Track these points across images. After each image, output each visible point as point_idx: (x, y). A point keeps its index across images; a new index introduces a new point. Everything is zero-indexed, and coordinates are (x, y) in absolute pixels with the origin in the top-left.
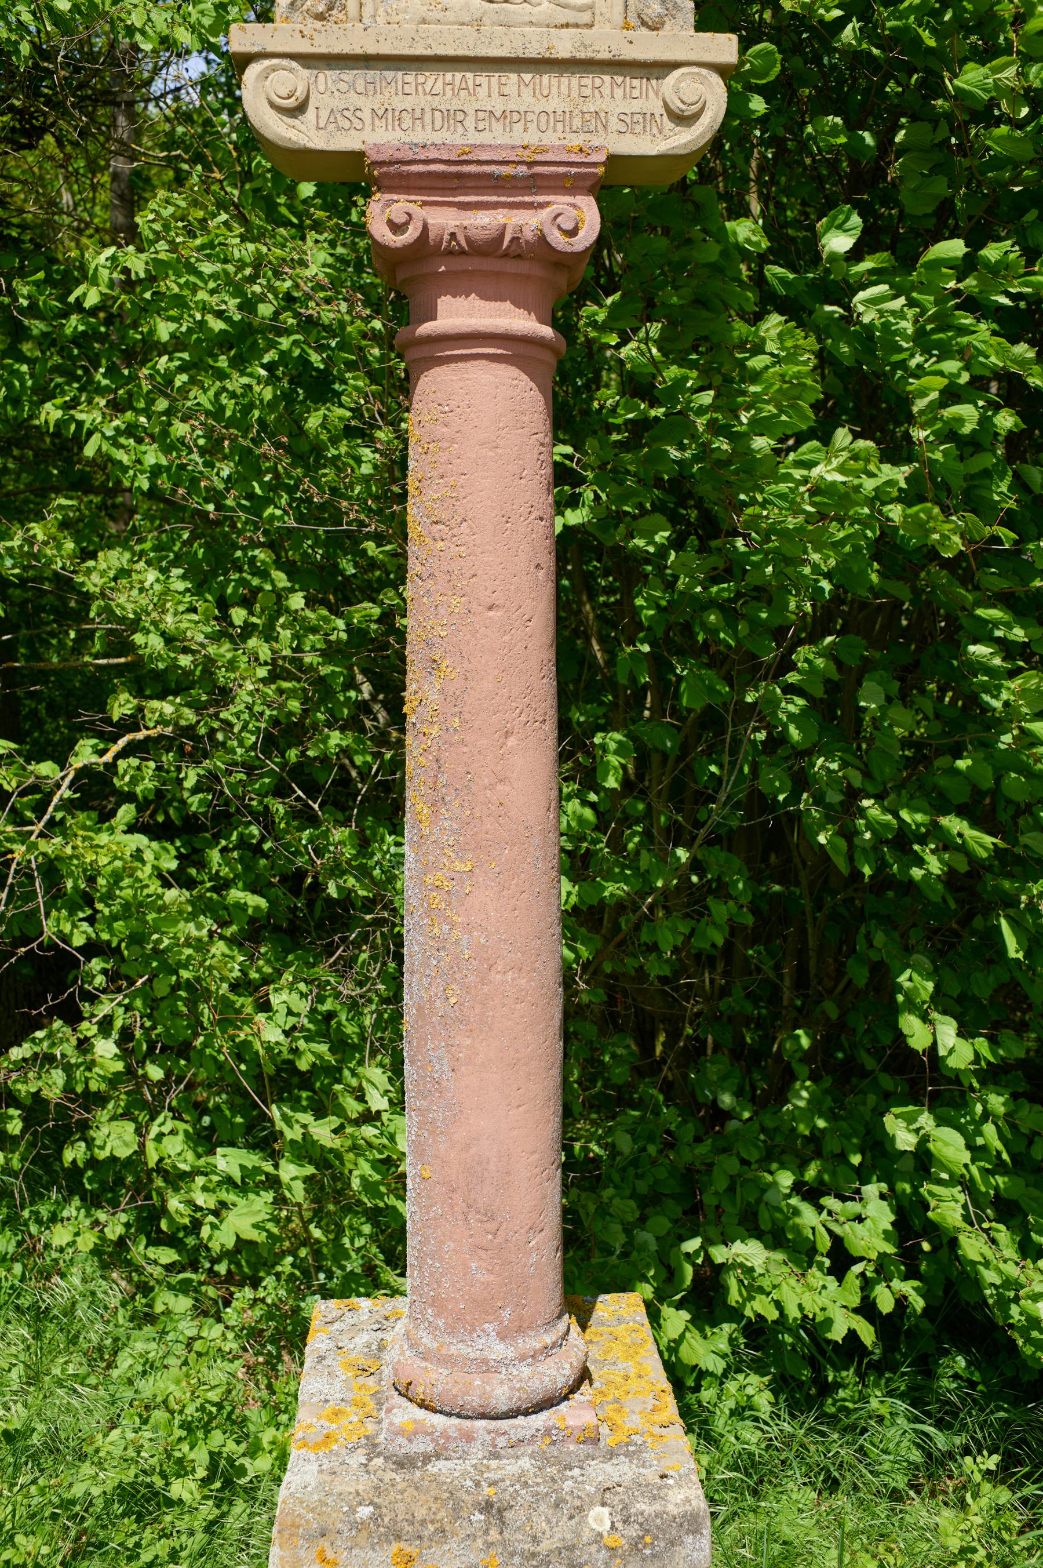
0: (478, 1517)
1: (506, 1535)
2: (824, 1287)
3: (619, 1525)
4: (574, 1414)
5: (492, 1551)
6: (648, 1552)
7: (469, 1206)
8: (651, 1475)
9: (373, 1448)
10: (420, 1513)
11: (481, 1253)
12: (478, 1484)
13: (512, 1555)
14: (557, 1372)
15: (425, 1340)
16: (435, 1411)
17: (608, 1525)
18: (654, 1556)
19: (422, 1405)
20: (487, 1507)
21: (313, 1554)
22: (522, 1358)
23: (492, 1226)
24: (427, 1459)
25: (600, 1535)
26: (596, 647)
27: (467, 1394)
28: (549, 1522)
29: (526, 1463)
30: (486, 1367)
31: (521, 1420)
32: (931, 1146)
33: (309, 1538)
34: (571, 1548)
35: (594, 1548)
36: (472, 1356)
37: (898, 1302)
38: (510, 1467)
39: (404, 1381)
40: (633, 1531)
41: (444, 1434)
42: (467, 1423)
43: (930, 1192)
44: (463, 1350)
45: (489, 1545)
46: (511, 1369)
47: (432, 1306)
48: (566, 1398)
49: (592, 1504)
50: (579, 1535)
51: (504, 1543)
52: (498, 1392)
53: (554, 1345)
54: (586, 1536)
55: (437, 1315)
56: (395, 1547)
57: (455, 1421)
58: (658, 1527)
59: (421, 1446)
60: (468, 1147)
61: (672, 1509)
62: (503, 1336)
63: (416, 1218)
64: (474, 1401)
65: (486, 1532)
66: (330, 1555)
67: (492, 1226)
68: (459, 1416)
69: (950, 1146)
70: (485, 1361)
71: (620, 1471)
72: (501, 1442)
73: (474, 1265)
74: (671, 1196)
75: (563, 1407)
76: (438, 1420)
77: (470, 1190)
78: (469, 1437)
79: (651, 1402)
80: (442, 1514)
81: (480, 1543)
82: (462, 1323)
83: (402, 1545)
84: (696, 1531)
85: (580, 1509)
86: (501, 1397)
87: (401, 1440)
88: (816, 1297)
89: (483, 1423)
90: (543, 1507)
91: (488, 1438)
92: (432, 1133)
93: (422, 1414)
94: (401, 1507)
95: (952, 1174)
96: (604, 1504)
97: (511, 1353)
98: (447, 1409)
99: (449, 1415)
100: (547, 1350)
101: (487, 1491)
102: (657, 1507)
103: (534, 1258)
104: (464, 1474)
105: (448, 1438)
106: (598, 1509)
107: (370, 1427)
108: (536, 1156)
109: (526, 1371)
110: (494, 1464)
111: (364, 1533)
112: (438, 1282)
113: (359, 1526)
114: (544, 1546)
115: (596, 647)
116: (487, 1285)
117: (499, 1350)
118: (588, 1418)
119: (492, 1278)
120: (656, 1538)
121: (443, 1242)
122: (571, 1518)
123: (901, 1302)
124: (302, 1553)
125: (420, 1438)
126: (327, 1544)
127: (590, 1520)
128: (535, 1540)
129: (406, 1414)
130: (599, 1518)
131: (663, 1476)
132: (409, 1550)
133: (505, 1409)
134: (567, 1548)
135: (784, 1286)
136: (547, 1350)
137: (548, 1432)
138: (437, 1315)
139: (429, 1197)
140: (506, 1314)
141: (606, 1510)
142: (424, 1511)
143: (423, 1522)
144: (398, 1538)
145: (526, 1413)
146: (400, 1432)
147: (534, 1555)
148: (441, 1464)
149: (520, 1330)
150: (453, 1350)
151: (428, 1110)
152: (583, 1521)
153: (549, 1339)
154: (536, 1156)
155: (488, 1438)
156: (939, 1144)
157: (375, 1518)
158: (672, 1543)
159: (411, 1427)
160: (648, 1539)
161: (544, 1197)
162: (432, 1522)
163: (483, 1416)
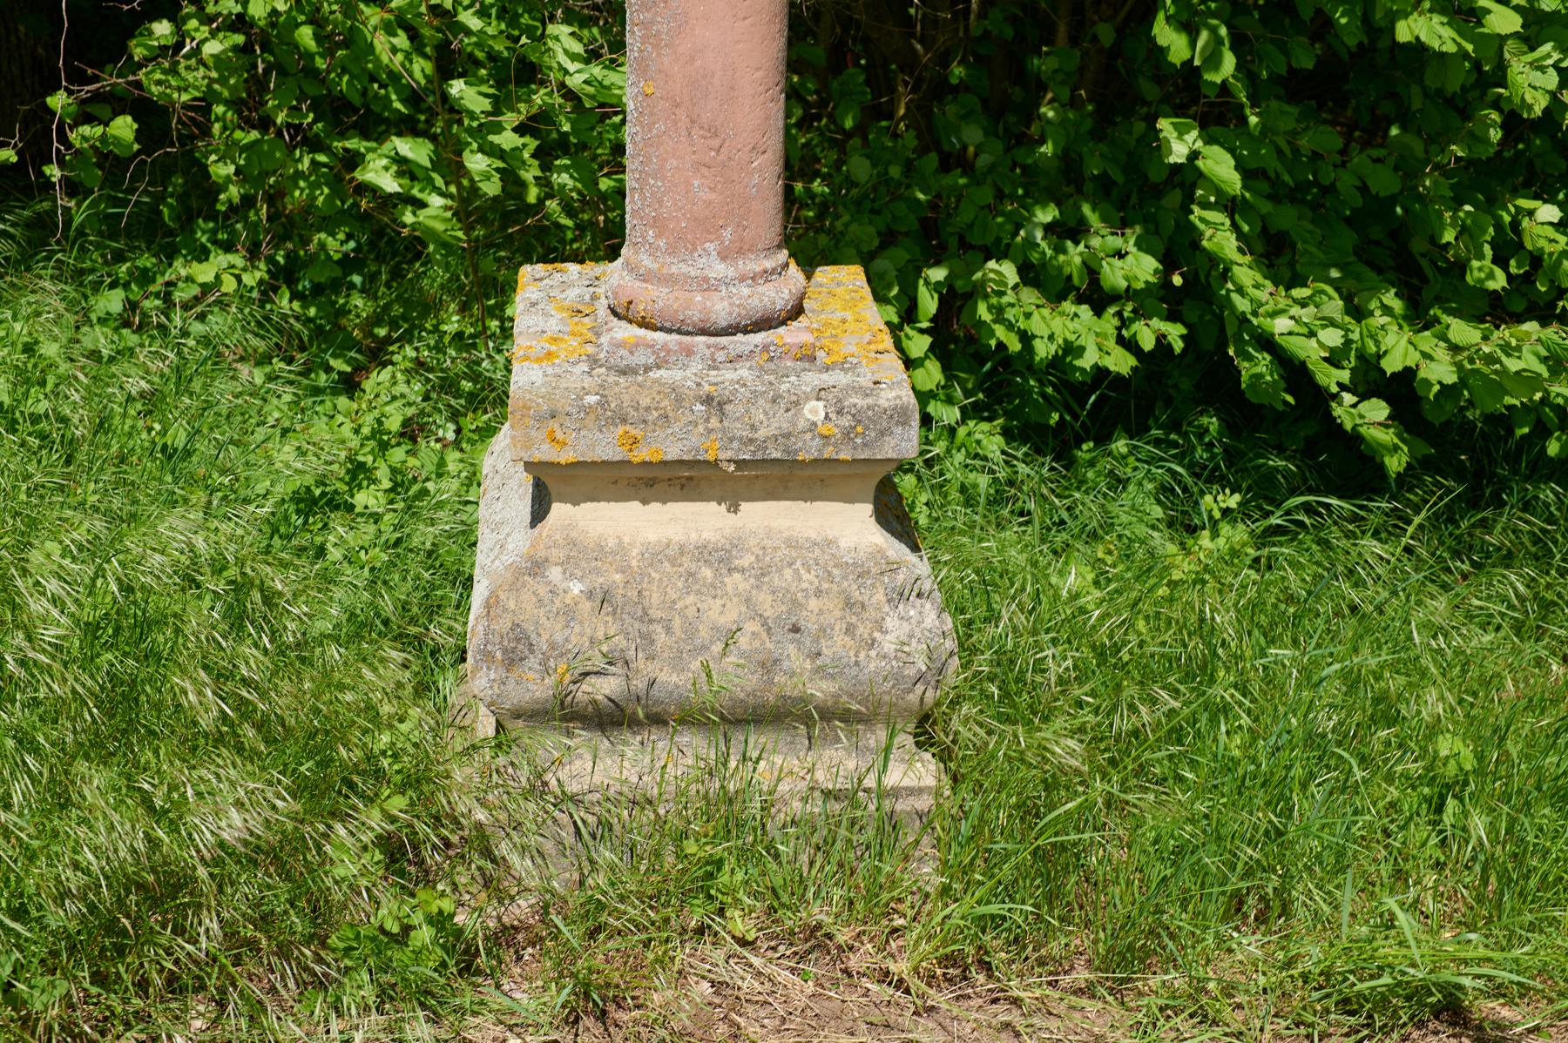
0: (699, 407)
1: (726, 423)
2: (1076, 315)
3: (833, 416)
4: (791, 335)
5: (713, 436)
6: (859, 441)
7: (693, 122)
8: (865, 381)
9: (594, 362)
10: (645, 401)
11: (704, 170)
12: (699, 384)
13: (731, 440)
14: (777, 295)
15: (646, 262)
16: (655, 328)
17: (823, 415)
18: (865, 445)
19: (644, 324)
20: (708, 400)
21: (543, 433)
22: (742, 279)
23: (716, 143)
24: (647, 369)
25: (815, 424)
26: (1093, 398)
27: (688, 308)
28: (766, 414)
29: (744, 373)
30: (707, 285)
31: (740, 337)
32: (1200, 163)
33: (540, 419)
34: (787, 436)
35: (808, 436)
36: (693, 274)
37: (1158, 340)
38: (729, 375)
39: (624, 301)
40: (846, 421)
41: (665, 347)
42: (688, 338)
43: (1202, 219)
44: (684, 268)
45: (710, 431)
46: (732, 288)
47: (652, 227)
48: (783, 323)
49: (808, 399)
50: (795, 425)
51: (723, 430)
52: (719, 307)
53: (773, 271)
54: (802, 424)
55: (658, 236)
56: (621, 429)
57: (675, 337)
58: (869, 418)
59: (640, 358)
60: (693, 59)
61: (883, 403)
62: (724, 256)
63: (638, 138)
64: (694, 316)
65: (707, 420)
66: (559, 435)
67: (716, 143)
68: (679, 332)
69: (1221, 166)
70: (706, 279)
71: (838, 378)
72: (721, 356)
73: (696, 183)
74: (907, 234)
75: (782, 330)
76: (660, 336)
77: (694, 105)
78: (689, 352)
79: (868, 337)
80: (666, 403)
81: (701, 428)
82: (683, 244)
83: (628, 428)
84: (905, 423)
85: (797, 403)
86: (721, 310)
87: (622, 352)
88: (1068, 323)
89: (703, 338)
90: (761, 402)
91: (708, 352)
92: (656, 46)
93: (642, 332)
94: (626, 397)
95: (1219, 192)
96: (818, 399)
97: (731, 272)
98: (668, 325)
99: (669, 331)
100: (767, 275)
101: (707, 387)
102: (870, 401)
103: (756, 179)
104: (684, 379)
105: (668, 351)
106: (814, 403)
107: (590, 349)
108: (760, 74)
109: (746, 291)
110: (713, 373)
111: (592, 416)
112: (660, 202)
113: (588, 410)
114: (762, 433)
115: (1093, 398)
116: (709, 203)
117: (719, 269)
118: (807, 338)
119: (714, 196)
120: (867, 428)
121: (665, 160)
122: (788, 410)
123: (1161, 338)
124: (533, 433)
125: (641, 350)
126: (556, 426)
127: (806, 412)
128: (753, 428)
129: (626, 331)
130: (814, 411)
131: (875, 383)
132: (633, 432)
133: (724, 324)
134: (783, 436)
135: (1036, 316)
136: (767, 275)
137: (766, 348)
138: (658, 236)
139: (652, 114)
140: (727, 234)
141: (821, 404)
142: (648, 400)
143: (648, 409)
144: (624, 421)
145: (746, 331)
146: (620, 345)
147: (751, 441)
148: (662, 372)
149: (740, 252)
150: (674, 269)
151: (652, 22)
152: (799, 413)
153: (769, 264)
154: (760, 74)
155: (708, 352)
156: (1209, 162)
157: (603, 404)
158: (882, 433)
159: (632, 341)
160: (859, 429)
161: (768, 118)
162: (656, 409)
163: (703, 332)
